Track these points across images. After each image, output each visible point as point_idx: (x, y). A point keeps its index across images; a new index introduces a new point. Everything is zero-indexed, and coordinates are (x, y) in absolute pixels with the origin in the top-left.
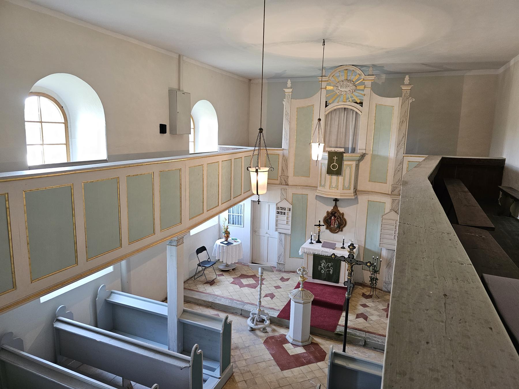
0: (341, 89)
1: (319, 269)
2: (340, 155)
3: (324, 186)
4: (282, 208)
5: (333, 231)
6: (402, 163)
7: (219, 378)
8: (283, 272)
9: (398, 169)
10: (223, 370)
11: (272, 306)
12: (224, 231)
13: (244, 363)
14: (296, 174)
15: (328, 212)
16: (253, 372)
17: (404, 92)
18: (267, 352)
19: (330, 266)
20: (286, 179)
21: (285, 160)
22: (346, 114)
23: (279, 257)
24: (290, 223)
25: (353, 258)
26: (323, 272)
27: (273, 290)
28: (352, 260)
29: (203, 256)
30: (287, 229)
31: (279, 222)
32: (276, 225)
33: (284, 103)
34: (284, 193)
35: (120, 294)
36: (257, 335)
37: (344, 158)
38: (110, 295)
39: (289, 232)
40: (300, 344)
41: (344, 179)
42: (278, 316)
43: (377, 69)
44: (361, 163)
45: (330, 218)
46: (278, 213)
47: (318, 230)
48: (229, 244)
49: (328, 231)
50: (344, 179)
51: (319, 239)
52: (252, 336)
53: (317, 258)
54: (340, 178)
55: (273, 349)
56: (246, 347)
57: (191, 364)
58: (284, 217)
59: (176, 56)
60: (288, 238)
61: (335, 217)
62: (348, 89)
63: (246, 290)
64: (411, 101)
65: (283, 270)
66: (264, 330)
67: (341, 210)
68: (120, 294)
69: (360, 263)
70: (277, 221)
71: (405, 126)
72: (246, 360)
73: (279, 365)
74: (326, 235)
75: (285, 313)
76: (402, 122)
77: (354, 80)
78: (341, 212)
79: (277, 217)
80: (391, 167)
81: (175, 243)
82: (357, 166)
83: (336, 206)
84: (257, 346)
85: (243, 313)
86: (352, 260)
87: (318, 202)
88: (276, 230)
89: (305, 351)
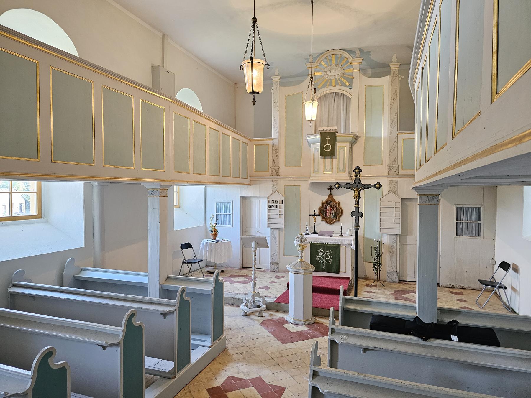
0: (330, 74)
1: (317, 259)
2: (333, 135)
3: (318, 172)
4: (274, 201)
5: (330, 222)
6: (396, 141)
7: (210, 347)
8: (277, 272)
9: (394, 148)
10: (214, 339)
11: (268, 295)
12: (211, 229)
13: (239, 340)
14: (288, 164)
15: (322, 202)
16: (249, 347)
17: (393, 71)
18: (265, 331)
19: (328, 254)
20: (277, 170)
21: (276, 149)
22: (336, 101)
23: (272, 256)
24: (283, 217)
25: (360, 183)
26: (321, 262)
27: (267, 284)
28: (359, 185)
29: (188, 253)
30: (280, 223)
31: (271, 216)
32: (268, 221)
33: (272, 91)
34: (276, 186)
35: (91, 270)
36: (252, 319)
37: (337, 138)
38: (80, 272)
39: (282, 227)
40: (303, 323)
41: (339, 162)
42: (275, 302)
43: (363, 53)
44: (355, 147)
45: (326, 208)
46: (270, 206)
47: (313, 221)
48: (217, 241)
49: (324, 223)
50: (339, 162)
51: (315, 231)
52: (246, 319)
53: (314, 248)
54: (334, 161)
55: (271, 328)
56: (240, 328)
57: (177, 307)
58: (277, 211)
59: (160, 35)
60: (282, 234)
61: (331, 206)
62: (337, 73)
63: (238, 285)
64: (400, 79)
65: (278, 270)
66: (261, 315)
67: (337, 198)
68: (91, 270)
69: (368, 186)
70: (269, 216)
71: (397, 105)
72: (240, 337)
73: (279, 340)
74: (322, 225)
75: (284, 299)
76: (393, 100)
77: (342, 64)
78: (337, 201)
79: (269, 211)
80: (385, 148)
81: (157, 194)
82: (351, 149)
83: (331, 195)
84: (252, 327)
85: (235, 303)
86: (359, 185)
87: (312, 192)
88: (268, 226)
89: (308, 329)
